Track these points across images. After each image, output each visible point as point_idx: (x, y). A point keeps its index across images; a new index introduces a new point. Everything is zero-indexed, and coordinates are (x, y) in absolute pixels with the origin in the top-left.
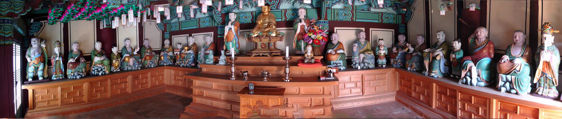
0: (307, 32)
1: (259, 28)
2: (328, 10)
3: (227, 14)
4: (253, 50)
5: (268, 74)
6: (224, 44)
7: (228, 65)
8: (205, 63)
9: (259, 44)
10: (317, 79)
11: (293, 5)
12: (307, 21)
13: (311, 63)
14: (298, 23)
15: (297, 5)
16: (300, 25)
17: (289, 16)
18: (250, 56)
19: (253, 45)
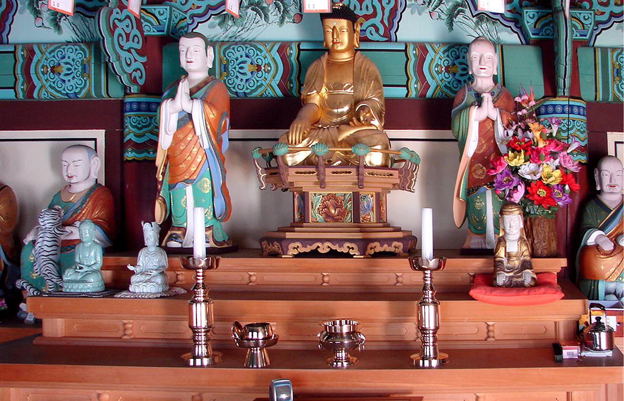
0: (503, 149)
1: (315, 124)
2: (581, 50)
3: (169, 40)
4: (291, 229)
5: (353, 333)
6: (154, 192)
7: (177, 296)
8: (58, 292)
9: (316, 199)
10: (547, 353)
11: (451, 24)
12: (502, 102)
13: (520, 286)
14: (468, 106)
15: (466, 28)
16: (476, 116)
17: (436, 79)
18: (275, 255)
19: (288, 205)
